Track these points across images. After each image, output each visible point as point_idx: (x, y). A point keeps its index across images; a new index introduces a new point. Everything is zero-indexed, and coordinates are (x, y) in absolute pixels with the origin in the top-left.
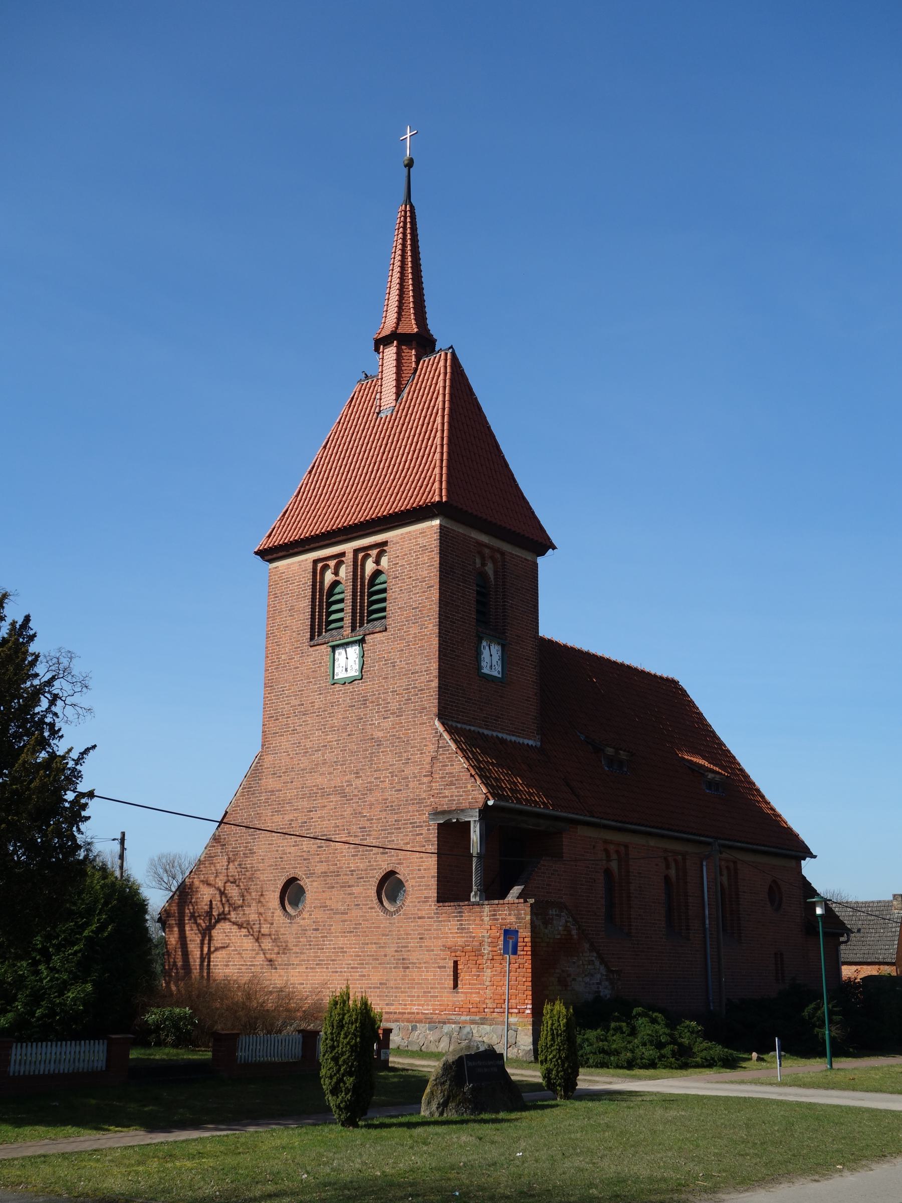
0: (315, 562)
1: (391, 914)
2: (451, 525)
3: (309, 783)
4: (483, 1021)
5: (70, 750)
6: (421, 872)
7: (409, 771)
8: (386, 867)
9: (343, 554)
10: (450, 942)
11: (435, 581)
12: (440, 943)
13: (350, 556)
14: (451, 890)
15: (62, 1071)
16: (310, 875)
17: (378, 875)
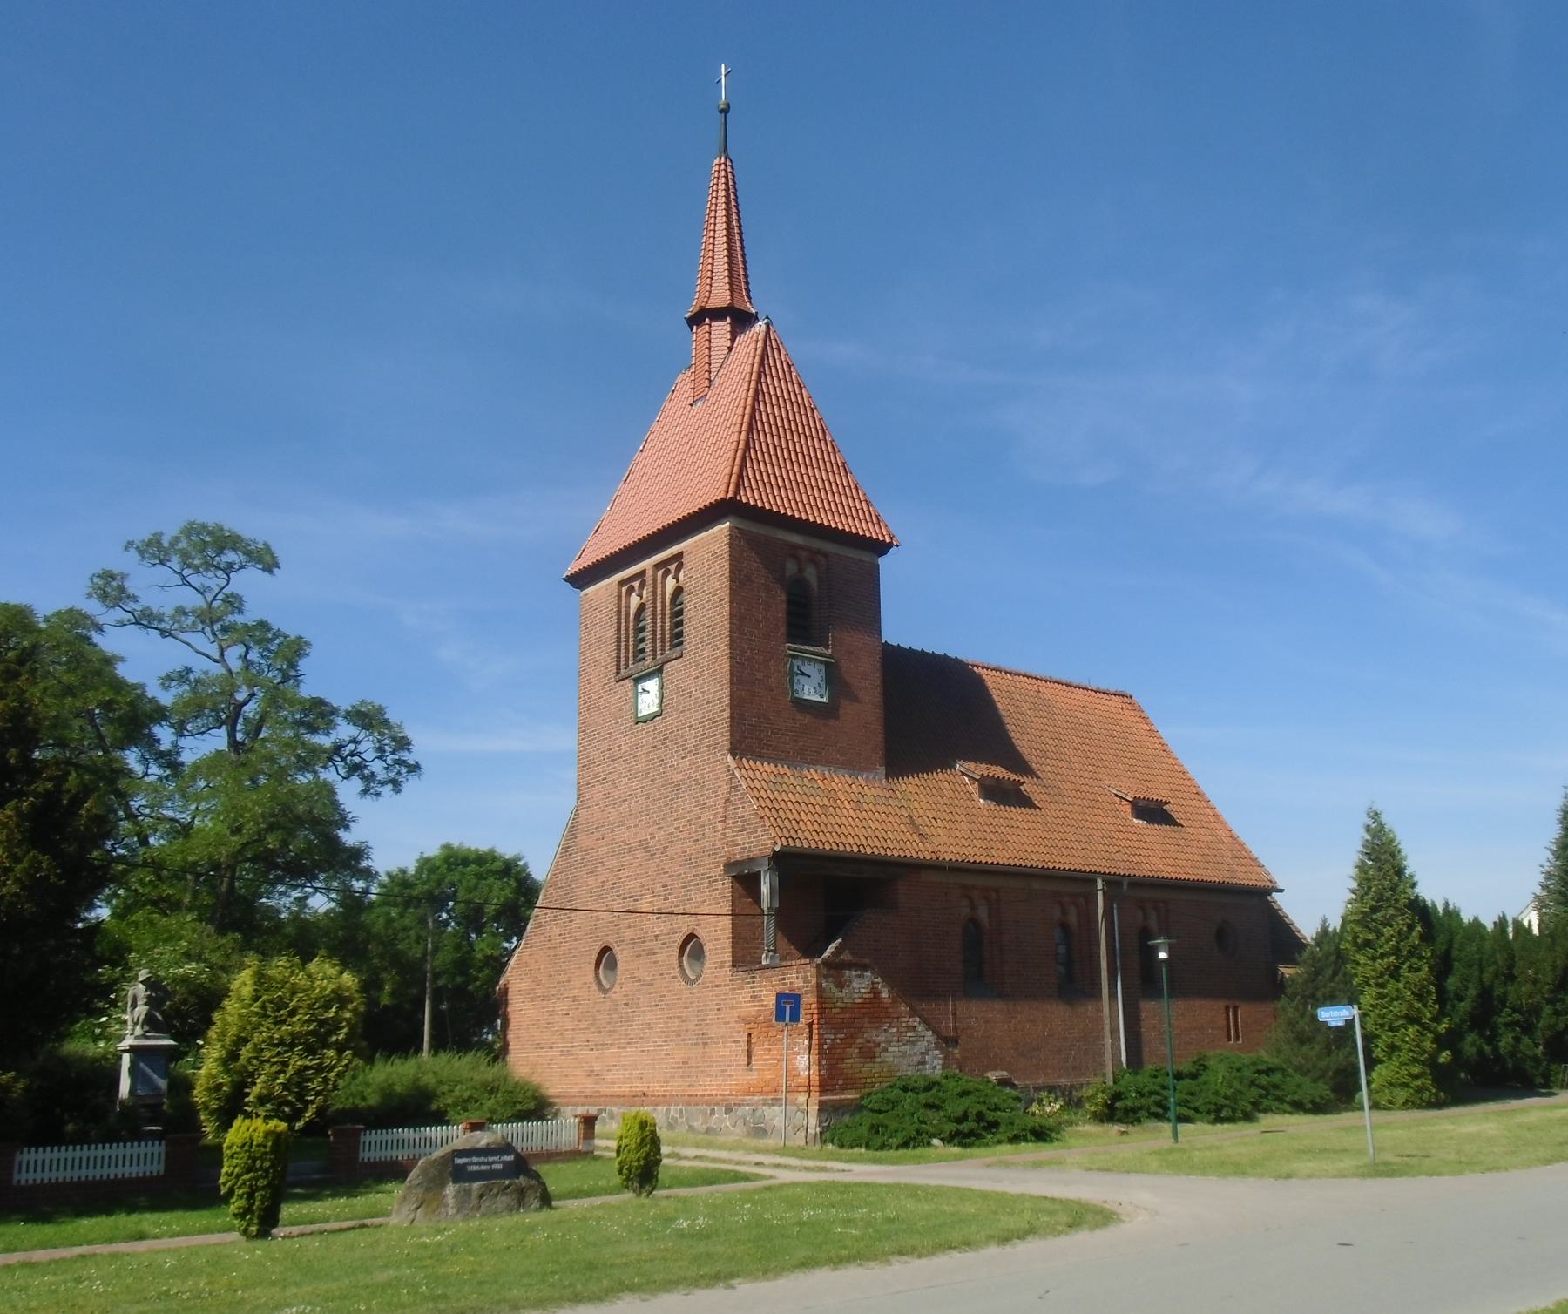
0: (622, 583)
1: (692, 982)
2: (746, 525)
3: (618, 838)
4: (776, 1102)
5: (266, 561)
6: (717, 936)
7: (706, 816)
8: (686, 930)
9: (643, 573)
10: (744, 1012)
11: (725, 594)
12: (735, 1013)
13: (650, 573)
14: (744, 958)
15: (23, 1182)
16: (620, 942)
17: (680, 938)
